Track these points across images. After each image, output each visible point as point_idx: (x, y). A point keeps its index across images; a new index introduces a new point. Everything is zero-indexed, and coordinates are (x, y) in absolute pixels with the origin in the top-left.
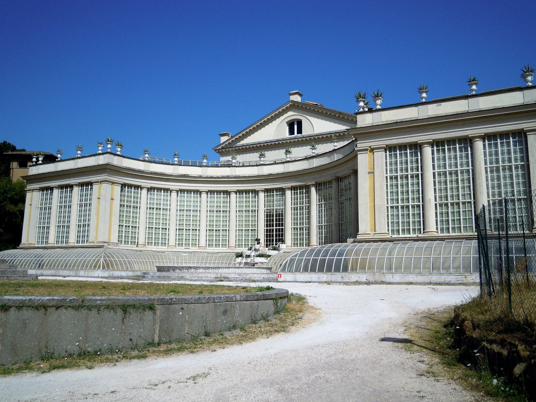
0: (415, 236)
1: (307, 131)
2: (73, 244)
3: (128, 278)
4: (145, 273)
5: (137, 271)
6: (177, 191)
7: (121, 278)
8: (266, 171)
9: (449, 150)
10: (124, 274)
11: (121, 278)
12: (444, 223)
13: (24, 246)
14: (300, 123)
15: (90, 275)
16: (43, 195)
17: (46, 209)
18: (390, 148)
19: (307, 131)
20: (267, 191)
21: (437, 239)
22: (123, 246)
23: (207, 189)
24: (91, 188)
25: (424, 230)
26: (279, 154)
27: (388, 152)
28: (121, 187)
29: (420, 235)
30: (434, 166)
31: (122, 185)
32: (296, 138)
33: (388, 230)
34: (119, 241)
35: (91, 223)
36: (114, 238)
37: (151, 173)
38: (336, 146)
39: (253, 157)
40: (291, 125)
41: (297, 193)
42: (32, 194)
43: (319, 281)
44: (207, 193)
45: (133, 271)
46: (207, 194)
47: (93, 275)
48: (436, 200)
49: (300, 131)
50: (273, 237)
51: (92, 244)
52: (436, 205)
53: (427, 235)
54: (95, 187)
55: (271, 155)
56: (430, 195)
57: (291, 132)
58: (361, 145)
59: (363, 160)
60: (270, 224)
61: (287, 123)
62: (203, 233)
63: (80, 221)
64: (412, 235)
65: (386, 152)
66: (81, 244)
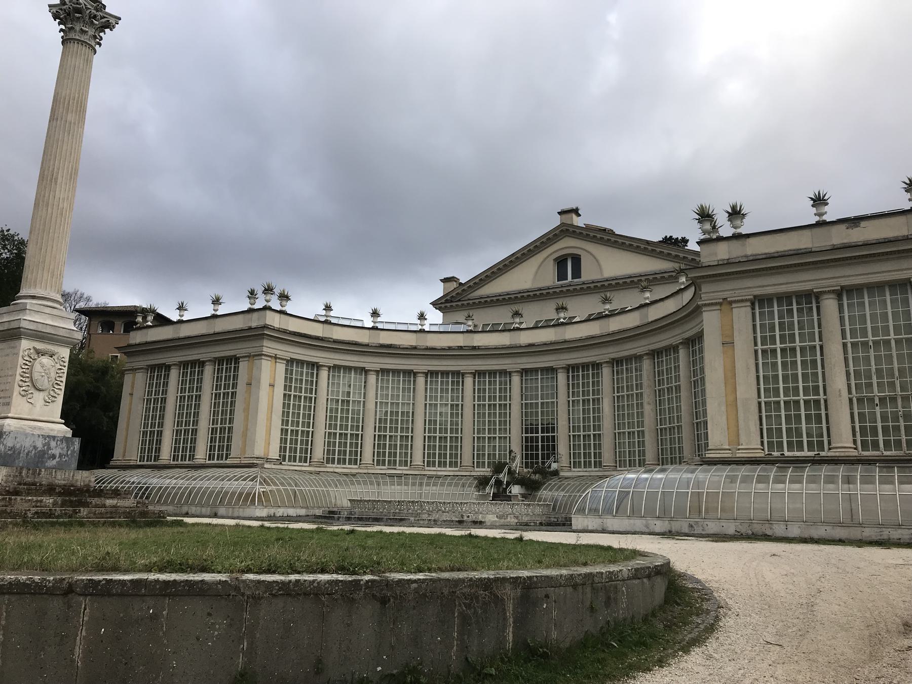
0: (811, 454)
1: (589, 273)
2: (202, 462)
3: (298, 519)
4: (331, 512)
5: (313, 508)
6: (426, 374)
7: (290, 519)
8: (525, 338)
9: (800, 311)
10: (292, 512)
11: (290, 519)
12: (865, 432)
13: (118, 463)
14: (577, 260)
15: (236, 514)
16: (152, 378)
17: (156, 404)
18: (760, 301)
19: (589, 273)
20: (524, 372)
21: (859, 460)
22: (287, 466)
23: (425, 369)
24: (236, 369)
25: (829, 443)
26: (547, 311)
27: (845, 298)
28: (287, 365)
29: (823, 454)
30: (843, 332)
31: (288, 361)
32: (584, 283)
33: (762, 443)
34: (280, 456)
35: (235, 425)
36: (274, 454)
37: (336, 342)
38: (648, 298)
39: (502, 316)
40: (561, 263)
41: (578, 376)
42: (134, 377)
43: (647, 531)
44: (426, 374)
45: (307, 508)
46: (427, 377)
47: (241, 514)
48: (850, 392)
49: (577, 273)
50: (537, 450)
51: (236, 461)
52: (851, 400)
53: (833, 454)
54: (243, 365)
55: (532, 313)
56: (838, 382)
57: (562, 275)
58: (710, 292)
59: (711, 321)
60: (532, 429)
61: (555, 260)
62: (418, 443)
63: (214, 422)
64: (806, 453)
65: (753, 309)
66: (215, 461)
